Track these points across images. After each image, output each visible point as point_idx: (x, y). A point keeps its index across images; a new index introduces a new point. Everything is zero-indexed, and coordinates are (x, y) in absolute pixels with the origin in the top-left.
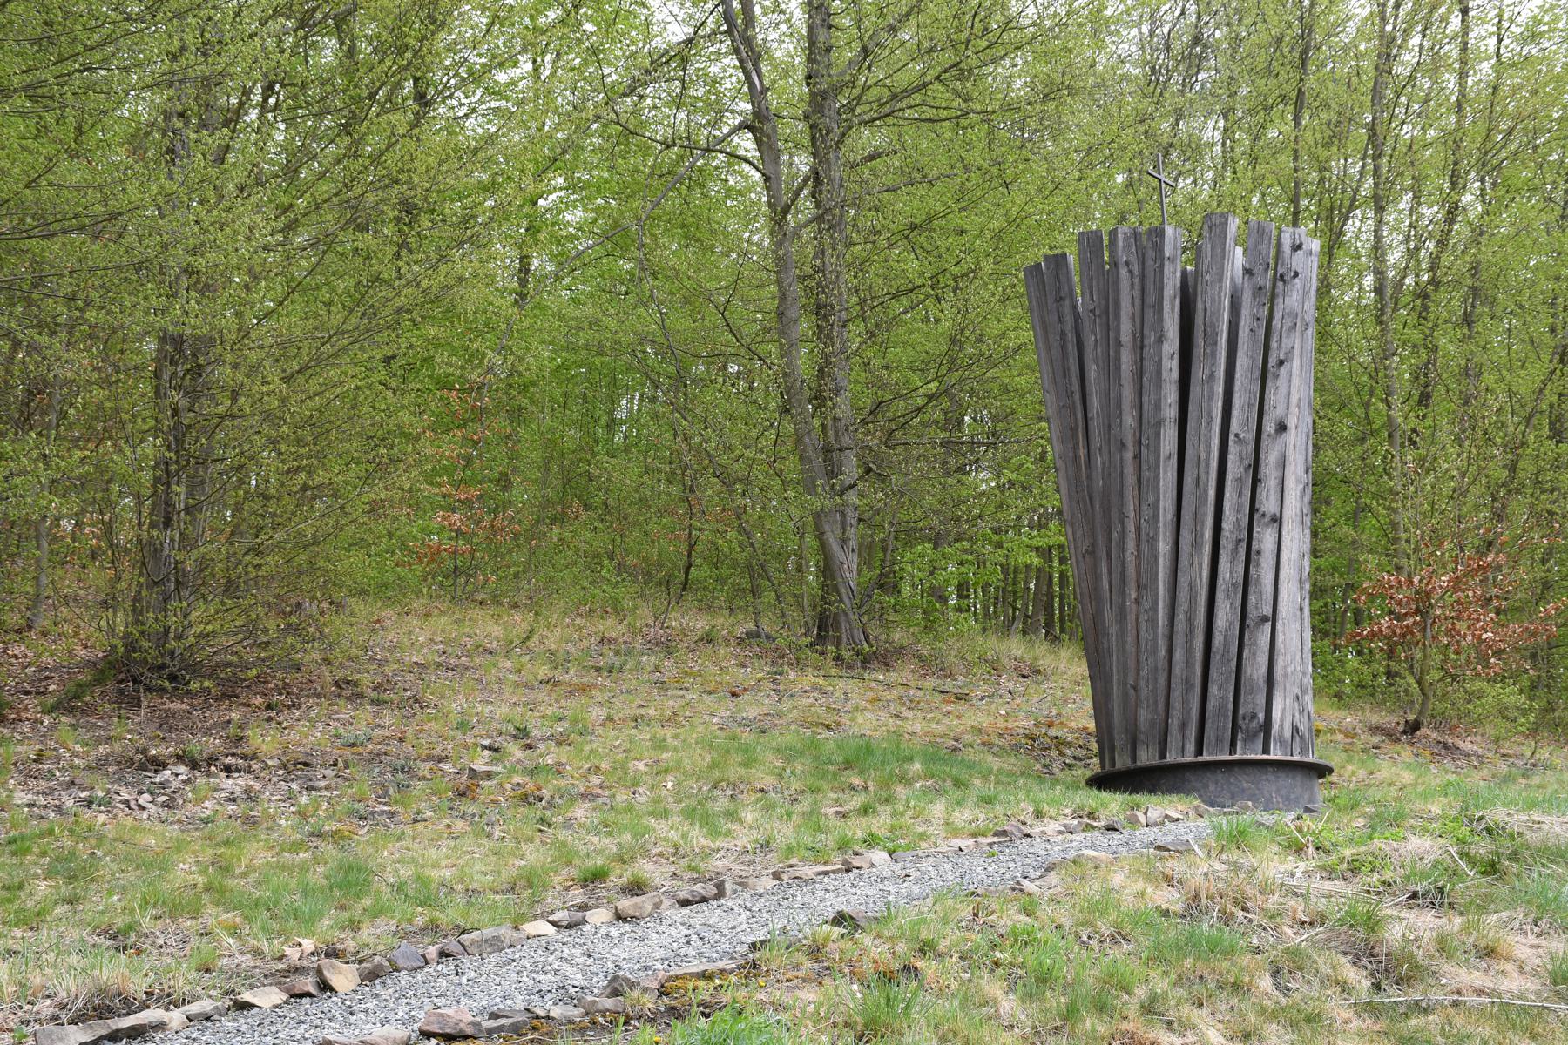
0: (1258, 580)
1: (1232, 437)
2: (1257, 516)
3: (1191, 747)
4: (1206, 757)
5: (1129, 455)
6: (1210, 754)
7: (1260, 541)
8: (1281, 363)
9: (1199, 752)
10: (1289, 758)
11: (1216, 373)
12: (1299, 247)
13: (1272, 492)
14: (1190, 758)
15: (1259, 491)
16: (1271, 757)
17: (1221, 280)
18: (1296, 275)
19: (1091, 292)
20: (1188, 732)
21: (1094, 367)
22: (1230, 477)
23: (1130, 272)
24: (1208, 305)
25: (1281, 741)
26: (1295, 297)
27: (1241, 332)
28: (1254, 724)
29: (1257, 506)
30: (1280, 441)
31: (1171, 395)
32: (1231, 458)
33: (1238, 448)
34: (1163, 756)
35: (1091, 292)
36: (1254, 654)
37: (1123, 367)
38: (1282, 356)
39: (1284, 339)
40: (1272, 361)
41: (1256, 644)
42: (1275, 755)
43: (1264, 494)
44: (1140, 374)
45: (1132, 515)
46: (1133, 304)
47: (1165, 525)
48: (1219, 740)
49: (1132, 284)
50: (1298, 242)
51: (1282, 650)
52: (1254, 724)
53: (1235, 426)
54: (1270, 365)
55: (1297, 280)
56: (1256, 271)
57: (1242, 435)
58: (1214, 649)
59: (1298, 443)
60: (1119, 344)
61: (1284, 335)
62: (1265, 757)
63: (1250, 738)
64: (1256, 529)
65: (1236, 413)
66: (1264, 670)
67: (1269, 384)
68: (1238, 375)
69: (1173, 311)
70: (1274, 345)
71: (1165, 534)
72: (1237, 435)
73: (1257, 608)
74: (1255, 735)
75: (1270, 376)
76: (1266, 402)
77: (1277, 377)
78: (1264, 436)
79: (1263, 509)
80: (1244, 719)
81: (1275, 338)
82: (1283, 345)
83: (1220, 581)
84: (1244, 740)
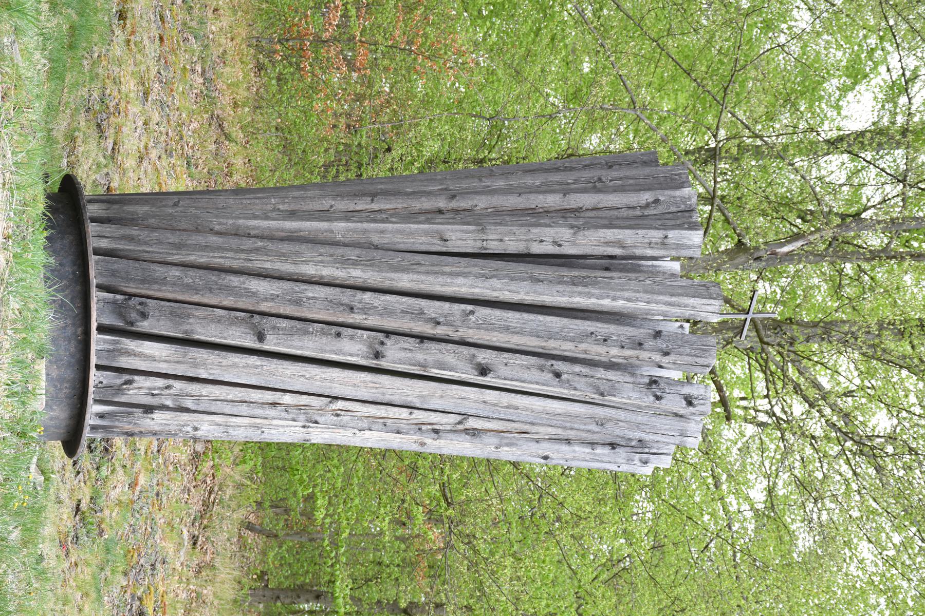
0: (306, 333)
1: (470, 307)
2: (381, 336)
3: (104, 244)
4: (93, 259)
5: (442, 203)
6: (97, 263)
7: (352, 337)
8: (558, 375)
9: (96, 252)
10: (91, 397)
11: (540, 287)
12: (690, 403)
13: (409, 355)
14: (93, 243)
15: (410, 340)
16: (93, 371)
17: (646, 292)
18: (658, 398)
19: (621, 179)
20: (122, 242)
21: (538, 183)
22: (424, 303)
23: (647, 206)
24: (617, 280)
25: (116, 352)
26: (633, 395)
27: (589, 323)
28: (134, 316)
29: (393, 337)
30: (469, 367)
31: (512, 245)
32: (447, 305)
33: (458, 313)
34: (93, 220)
35: (621, 179)
36: (219, 321)
37: (541, 197)
38: (564, 377)
39: (584, 380)
40: (560, 366)
41: (231, 324)
42: (98, 342)
43: (406, 345)
44: (532, 212)
45: (375, 207)
46: (611, 208)
47: (365, 231)
48: (114, 274)
49: (634, 208)
50: (695, 402)
51: (225, 362)
52: (134, 316)
53: (484, 312)
54: (553, 362)
55: (652, 398)
56: (659, 341)
57: (472, 318)
58: (223, 275)
59: (465, 402)
60: (570, 297)
61: (590, 380)
62: (94, 325)
63: (119, 310)
64: (366, 333)
65: (497, 313)
66: (201, 335)
67: (533, 360)
68: (540, 318)
69: (607, 243)
70: (577, 368)
71: (355, 231)
72: (472, 312)
73: (274, 328)
74: (121, 316)
75: (541, 361)
76: (511, 355)
77: (541, 369)
78: (473, 350)
79: (389, 342)
80: (141, 304)
81: (585, 370)
82: (577, 379)
83: (304, 286)
84: (114, 302)
